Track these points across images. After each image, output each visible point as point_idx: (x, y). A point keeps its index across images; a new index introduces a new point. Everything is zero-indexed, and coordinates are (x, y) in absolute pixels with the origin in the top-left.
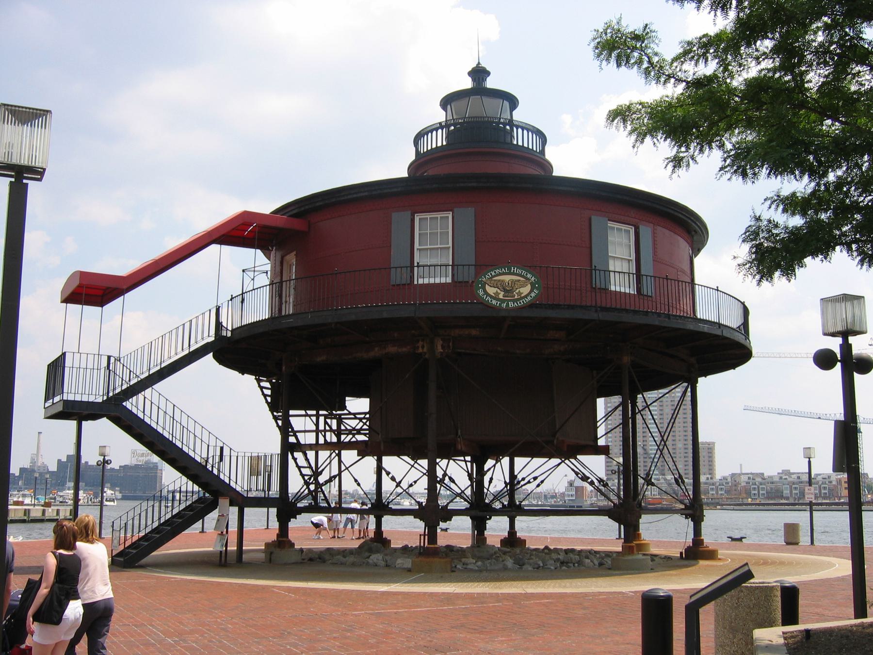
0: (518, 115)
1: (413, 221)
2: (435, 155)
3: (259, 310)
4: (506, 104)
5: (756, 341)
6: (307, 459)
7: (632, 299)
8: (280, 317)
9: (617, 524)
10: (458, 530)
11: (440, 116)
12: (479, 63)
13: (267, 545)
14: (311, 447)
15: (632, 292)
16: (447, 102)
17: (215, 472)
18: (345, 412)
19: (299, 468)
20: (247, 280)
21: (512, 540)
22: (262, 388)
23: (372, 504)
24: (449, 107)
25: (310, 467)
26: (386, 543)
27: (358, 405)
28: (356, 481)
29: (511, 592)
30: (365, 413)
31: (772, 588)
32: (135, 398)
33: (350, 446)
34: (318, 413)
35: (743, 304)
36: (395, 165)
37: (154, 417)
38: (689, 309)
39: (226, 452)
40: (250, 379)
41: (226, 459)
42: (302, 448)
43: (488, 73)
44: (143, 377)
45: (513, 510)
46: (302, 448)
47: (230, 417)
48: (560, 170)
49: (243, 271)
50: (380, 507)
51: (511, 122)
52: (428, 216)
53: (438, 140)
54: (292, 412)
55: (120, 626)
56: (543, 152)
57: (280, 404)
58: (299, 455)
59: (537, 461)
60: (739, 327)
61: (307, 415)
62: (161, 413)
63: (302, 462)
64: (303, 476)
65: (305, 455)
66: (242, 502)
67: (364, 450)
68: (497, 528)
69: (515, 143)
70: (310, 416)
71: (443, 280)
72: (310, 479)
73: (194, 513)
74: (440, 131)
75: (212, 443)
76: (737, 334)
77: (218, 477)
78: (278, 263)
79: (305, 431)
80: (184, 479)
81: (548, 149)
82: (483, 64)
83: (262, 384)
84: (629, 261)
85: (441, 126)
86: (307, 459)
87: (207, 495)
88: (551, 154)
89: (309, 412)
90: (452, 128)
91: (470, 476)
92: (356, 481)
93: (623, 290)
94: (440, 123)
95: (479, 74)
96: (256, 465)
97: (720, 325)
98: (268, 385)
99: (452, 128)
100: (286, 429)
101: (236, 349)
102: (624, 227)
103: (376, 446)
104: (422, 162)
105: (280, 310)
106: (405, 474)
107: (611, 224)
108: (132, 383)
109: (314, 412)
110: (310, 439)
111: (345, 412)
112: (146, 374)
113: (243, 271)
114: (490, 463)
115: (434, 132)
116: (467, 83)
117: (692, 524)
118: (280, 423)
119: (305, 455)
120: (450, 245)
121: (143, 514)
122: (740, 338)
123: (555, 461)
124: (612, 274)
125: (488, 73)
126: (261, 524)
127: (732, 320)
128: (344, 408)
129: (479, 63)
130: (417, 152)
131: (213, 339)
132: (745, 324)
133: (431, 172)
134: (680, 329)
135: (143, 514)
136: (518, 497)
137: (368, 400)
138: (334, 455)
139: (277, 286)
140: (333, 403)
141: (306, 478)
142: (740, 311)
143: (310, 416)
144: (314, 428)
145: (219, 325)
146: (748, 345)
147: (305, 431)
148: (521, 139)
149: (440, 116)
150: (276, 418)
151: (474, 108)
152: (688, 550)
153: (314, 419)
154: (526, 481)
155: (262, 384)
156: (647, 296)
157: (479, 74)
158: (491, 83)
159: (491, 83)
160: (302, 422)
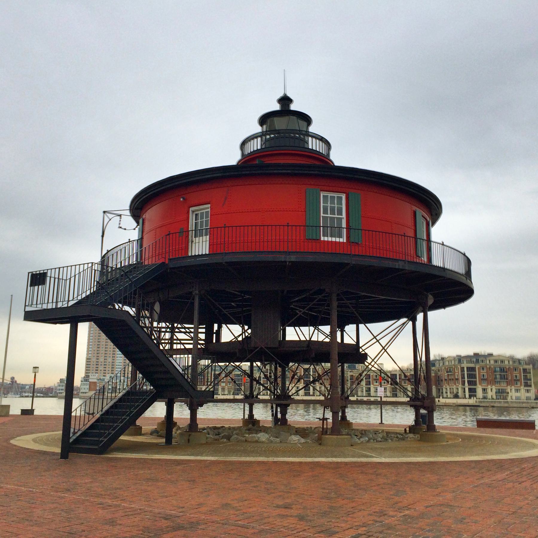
0: (312, 129)
1: (188, 212)
2: (255, 155)
5: (476, 282)
11: (258, 129)
16: (264, 120)
28: (103, 236)
29: (281, 458)
35: (468, 262)
36: (232, 157)
38: (425, 259)
48: (336, 164)
49: (104, 212)
51: (308, 134)
52: (330, 194)
53: (256, 145)
56: (328, 154)
69: (310, 147)
71: (341, 240)
81: (332, 153)
82: (289, 95)
88: (332, 157)
95: (285, 101)
116: (277, 107)
121: (73, 279)
122: (464, 280)
127: (455, 265)
130: (243, 154)
134: (440, 277)
135: (73, 279)
138: (115, 267)
146: (470, 285)
148: (313, 144)
149: (258, 129)
151: (280, 123)
157: (285, 101)
158: (293, 107)
159: (293, 107)
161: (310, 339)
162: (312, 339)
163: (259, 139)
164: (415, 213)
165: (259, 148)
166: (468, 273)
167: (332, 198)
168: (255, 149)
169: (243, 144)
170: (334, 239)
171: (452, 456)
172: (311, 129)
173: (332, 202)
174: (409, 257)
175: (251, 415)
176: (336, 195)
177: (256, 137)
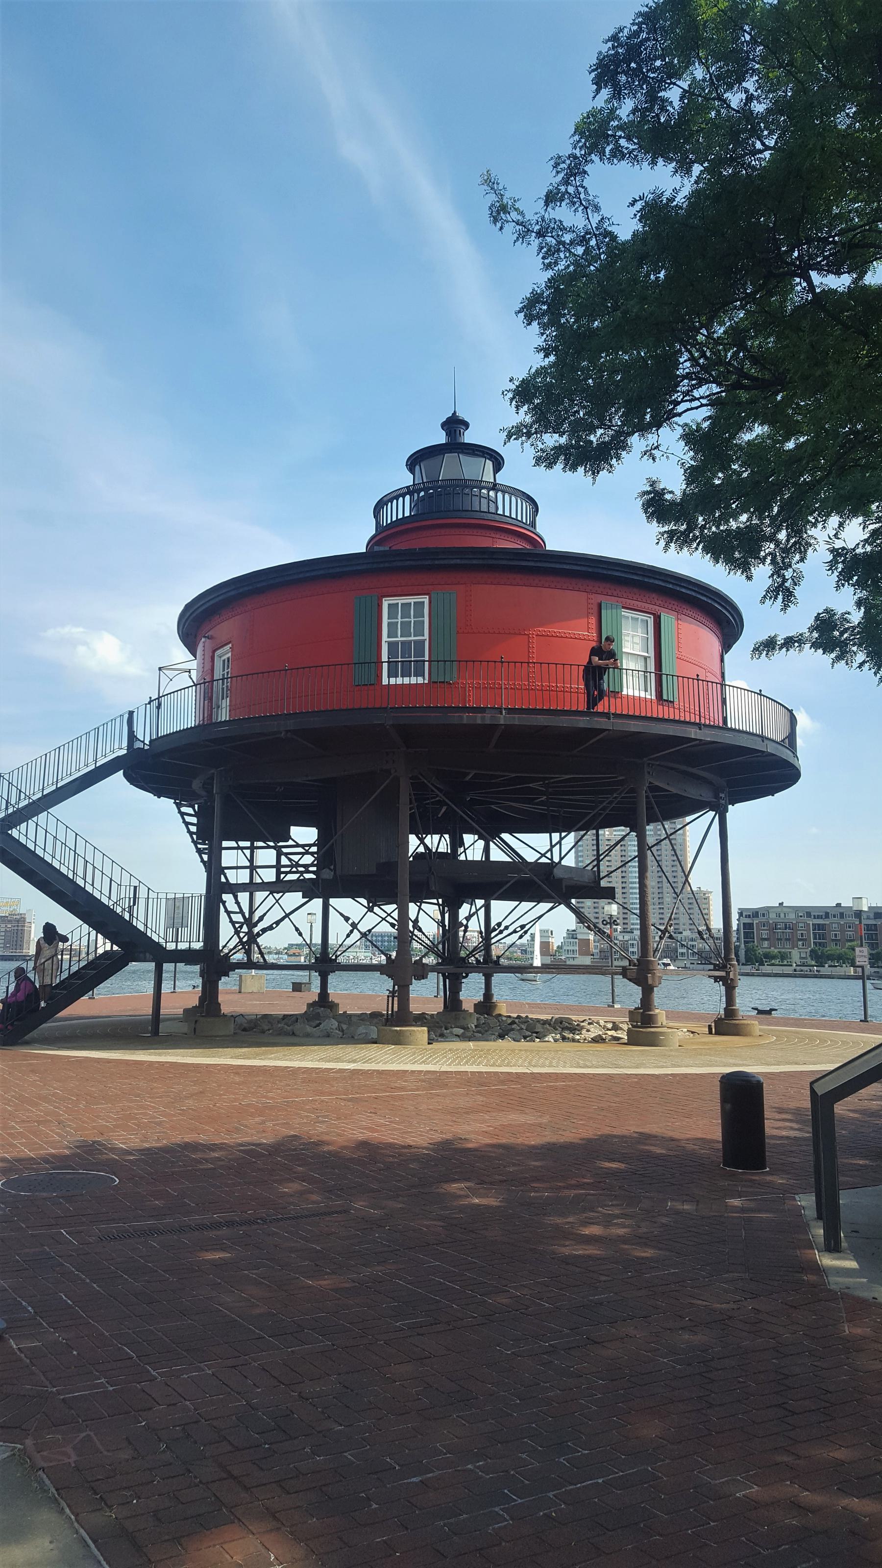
3: (182, 716)
4: (489, 464)
6: (238, 903)
7: (649, 704)
8: (212, 724)
9: (265, 881)
10: (426, 994)
11: (406, 479)
12: (455, 412)
13: (185, 1010)
14: (243, 887)
15: (648, 697)
16: (413, 462)
17: (127, 916)
18: (291, 842)
19: (228, 913)
20: (164, 680)
21: (486, 1005)
22: (182, 814)
23: (316, 958)
24: (417, 467)
25: (241, 912)
26: (333, 1006)
27: (305, 834)
28: (297, 929)
30: (310, 846)
31: (716, 1034)
32: (24, 825)
33: (291, 887)
34: (252, 844)
35: (791, 711)
37: (49, 849)
39: (142, 893)
40: (168, 804)
41: (142, 902)
42: (234, 889)
43: (466, 425)
44: (35, 798)
45: (490, 966)
46: (234, 889)
47: (146, 851)
48: (552, 545)
49: (160, 669)
50: (325, 962)
52: (400, 601)
53: (403, 509)
54: (225, 844)
55: (16, 1122)
56: (533, 524)
57: (208, 838)
58: (228, 898)
59: (526, 905)
60: (782, 741)
61: (238, 848)
62: (50, 839)
63: (231, 905)
64: (233, 923)
65: (236, 897)
66: (160, 956)
67: (310, 890)
68: (472, 990)
70: (242, 849)
71: (420, 680)
72: (241, 927)
73: (101, 969)
74: (408, 497)
75: (125, 882)
76: (780, 747)
77: (129, 923)
78: (208, 659)
79: (237, 868)
80: (86, 927)
82: (461, 414)
83: (183, 809)
84: (646, 658)
85: (409, 491)
86: (238, 903)
87: (115, 948)
89: (242, 844)
90: (422, 494)
91: (441, 923)
92: (297, 929)
93: (637, 694)
94: (408, 487)
95: (454, 425)
96: (177, 908)
97: (763, 738)
98: (190, 810)
99: (422, 494)
100: (214, 868)
101: (155, 766)
102: (641, 616)
103: (323, 886)
104: (385, 534)
105: (210, 716)
106: (354, 921)
107: (625, 613)
108: (21, 805)
109: (248, 844)
110: (243, 877)
111: (291, 842)
112: (40, 795)
113: (160, 669)
114: (464, 910)
115: (401, 499)
116: (441, 438)
117: (723, 988)
118: (205, 857)
119: (236, 897)
120: (426, 636)
122: (786, 754)
123: (544, 906)
124: (624, 671)
125: (466, 425)
126: (184, 987)
127: (775, 731)
128: (288, 837)
129: (455, 412)
131: (125, 752)
132: (792, 737)
133: (401, 545)
136: (495, 951)
137: (292, 828)
139: (206, 686)
140: (278, 835)
141: (237, 925)
142: (785, 720)
143: (242, 849)
144: (248, 864)
145: (132, 737)
146: (795, 763)
147: (237, 868)
148: (509, 508)
150: (200, 852)
152: (718, 1022)
153: (247, 852)
154: (511, 929)
155: (183, 809)
156: (667, 701)
157: (454, 425)
158: (469, 437)
160: (232, 857)
161: (560, 862)
162: (563, 863)
163: (408, 497)
164: (769, 645)
165: (407, 514)
166: (791, 740)
167: (406, 606)
168: (400, 516)
169: (380, 505)
170: (406, 680)
171: (59, 1049)
172: (502, 478)
173: (406, 626)
174: (687, 714)
175: (488, 995)
176: (412, 600)
177: (403, 495)
